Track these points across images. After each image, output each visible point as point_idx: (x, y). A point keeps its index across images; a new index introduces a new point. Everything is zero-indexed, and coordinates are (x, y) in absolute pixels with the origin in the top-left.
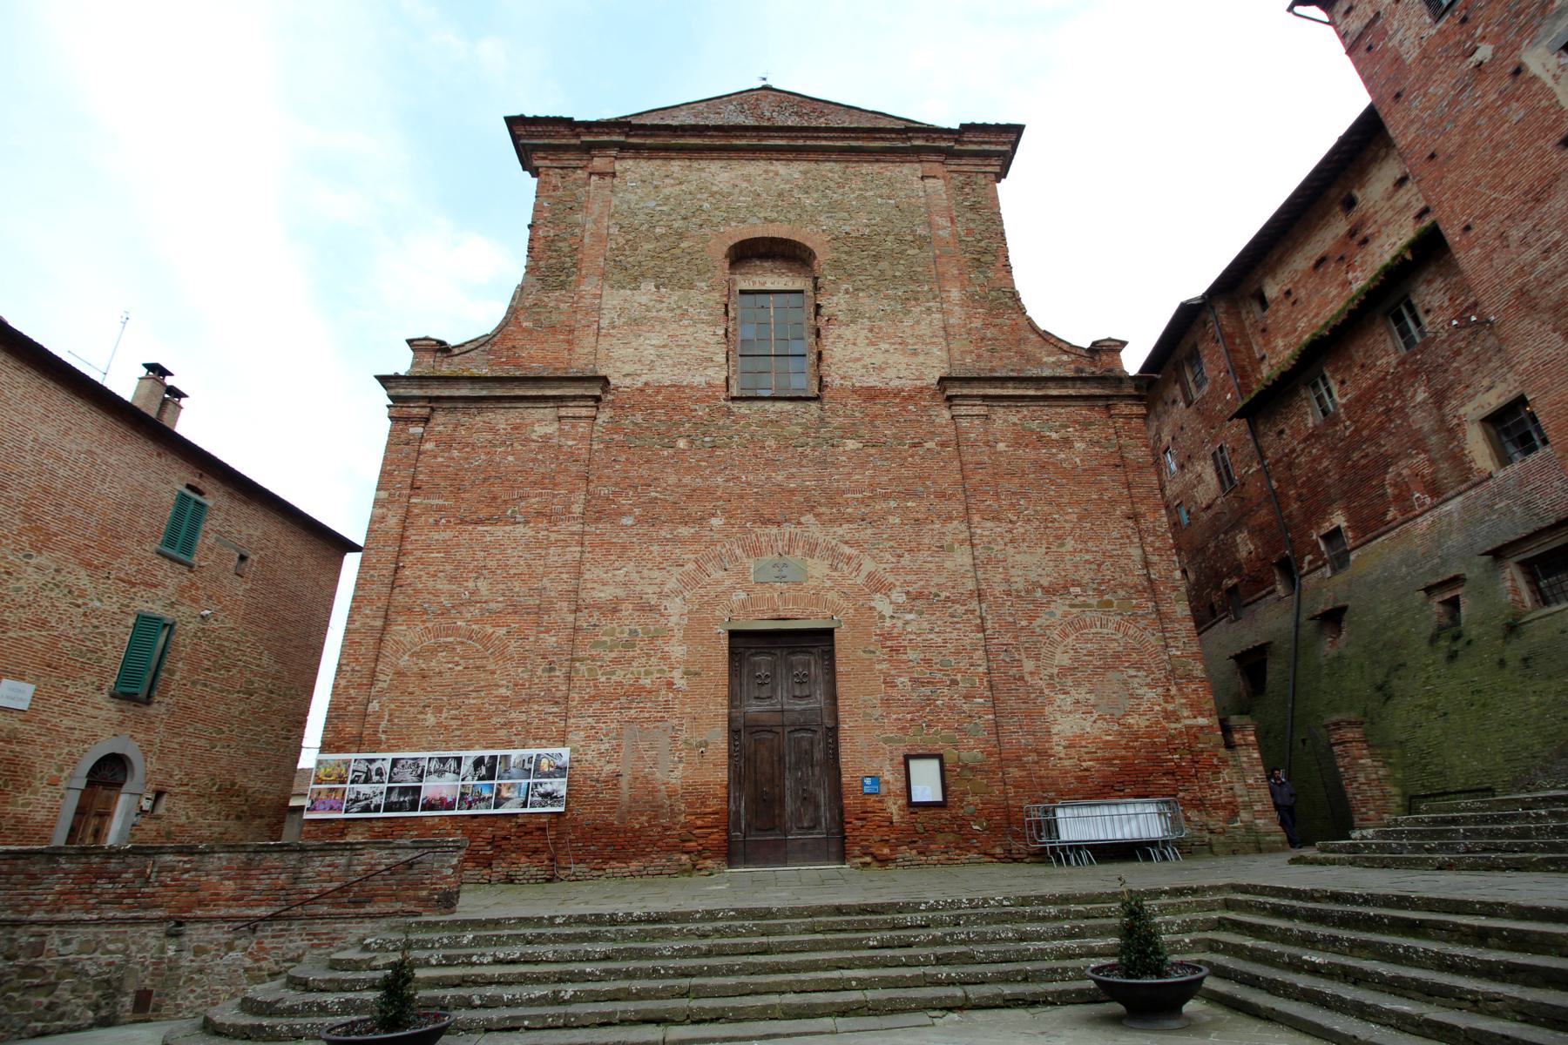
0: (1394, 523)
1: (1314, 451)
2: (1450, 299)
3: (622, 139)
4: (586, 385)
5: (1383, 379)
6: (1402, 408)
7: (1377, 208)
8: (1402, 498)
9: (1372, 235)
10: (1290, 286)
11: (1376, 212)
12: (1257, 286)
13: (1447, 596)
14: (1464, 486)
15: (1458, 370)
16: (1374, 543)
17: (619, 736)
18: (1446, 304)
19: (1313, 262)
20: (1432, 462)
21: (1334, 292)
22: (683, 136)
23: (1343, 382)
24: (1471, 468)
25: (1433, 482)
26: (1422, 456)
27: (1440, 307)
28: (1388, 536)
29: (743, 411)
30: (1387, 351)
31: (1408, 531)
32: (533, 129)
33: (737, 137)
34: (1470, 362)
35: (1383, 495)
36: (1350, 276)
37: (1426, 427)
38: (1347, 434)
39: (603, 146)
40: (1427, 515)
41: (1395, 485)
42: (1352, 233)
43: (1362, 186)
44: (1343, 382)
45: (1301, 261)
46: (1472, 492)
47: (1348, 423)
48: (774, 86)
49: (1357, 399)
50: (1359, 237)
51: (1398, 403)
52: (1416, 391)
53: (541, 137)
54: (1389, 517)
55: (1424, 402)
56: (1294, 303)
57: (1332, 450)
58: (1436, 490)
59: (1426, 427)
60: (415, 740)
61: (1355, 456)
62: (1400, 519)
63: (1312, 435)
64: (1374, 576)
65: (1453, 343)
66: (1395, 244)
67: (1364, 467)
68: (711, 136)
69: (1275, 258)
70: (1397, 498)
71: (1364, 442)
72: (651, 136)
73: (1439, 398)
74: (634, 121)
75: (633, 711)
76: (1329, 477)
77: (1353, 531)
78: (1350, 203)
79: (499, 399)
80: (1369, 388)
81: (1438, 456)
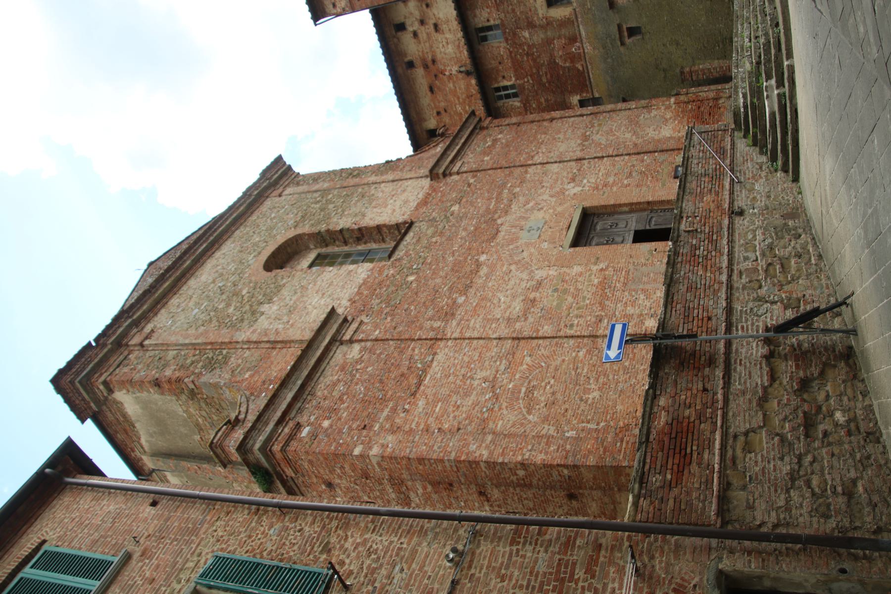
0: (584, 65)
1: (534, 106)
2: (487, 8)
3: (130, 320)
4: (332, 321)
5: (511, 52)
6: (529, 46)
7: (421, 50)
8: (573, 58)
9: (433, 56)
10: (435, 112)
11: (423, 51)
12: (425, 133)
13: (626, 34)
14: (576, 23)
15: (521, 12)
16: (592, 80)
17: (636, 291)
18: (489, 10)
19: (429, 94)
20: (559, 37)
21: (451, 85)
22: (157, 290)
23: (504, 77)
24: (568, 19)
25: (570, 39)
26: (555, 41)
27: (489, 13)
28: (590, 71)
29: (401, 254)
30: (498, 47)
31: (590, 58)
32: (74, 370)
33: (182, 264)
34: (520, 6)
35: (569, 68)
36: (447, 73)
37: (542, 36)
38: (531, 82)
39: (125, 334)
40: (585, 46)
41: (565, 61)
42: (426, 67)
43: (405, 55)
44: (504, 77)
45: (425, 99)
46: (580, 20)
47: (526, 80)
48: (153, 260)
49: (516, 71)
50: (430, 64)
51: (526, 48)
52: (523, 36)
53: (84, 368)
54: (580, 68)
55: (530, 33)
56: (445, 111)
57: (537, 94)
58: (573, 39)
59: (542, 36)
60: (610, 403)
61: (544, 80)
62: (583, 62)
63: (525, 105)
64: (609, 79)
65: (508, 13)
66: (443, 45)
67: (552, 77)
68: (170, 276)
69: (415, 116)
70: (572, 62)
71: (539, 73)
72: (142, 305)
73: (531, 25)
74: (125, 308)
75: (618, 285)
76: (551, 100)
77: (582, 92)
78: (411, 65)
79: (309, 377)
80: (513, 62)
81: (558, 33)
